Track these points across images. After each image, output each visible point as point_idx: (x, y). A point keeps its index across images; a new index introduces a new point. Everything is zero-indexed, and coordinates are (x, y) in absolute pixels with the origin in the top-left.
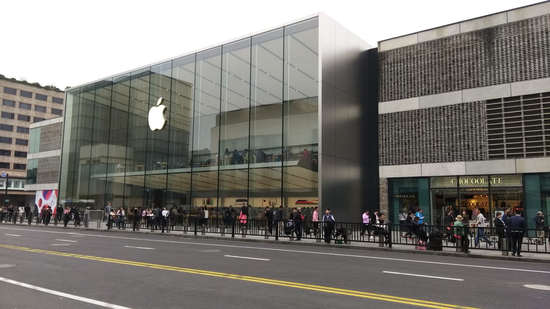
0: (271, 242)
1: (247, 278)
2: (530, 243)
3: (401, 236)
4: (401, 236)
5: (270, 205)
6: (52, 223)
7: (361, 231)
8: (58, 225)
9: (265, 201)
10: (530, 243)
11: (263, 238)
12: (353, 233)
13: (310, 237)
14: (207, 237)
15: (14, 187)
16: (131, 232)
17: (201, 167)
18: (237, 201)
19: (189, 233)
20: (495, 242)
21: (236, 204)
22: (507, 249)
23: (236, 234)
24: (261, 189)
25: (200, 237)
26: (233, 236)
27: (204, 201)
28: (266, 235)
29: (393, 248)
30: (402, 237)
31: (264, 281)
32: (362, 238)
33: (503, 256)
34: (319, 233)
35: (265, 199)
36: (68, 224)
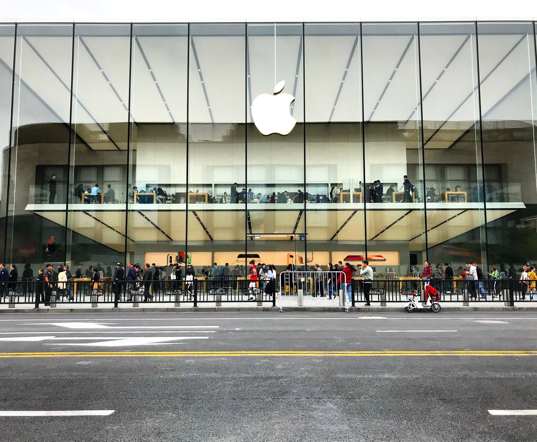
0: (266, 310)
1: (109, 354)
2: (373, 294)
3: (85, 294)
4: (85, 294)
5: (302, 263)
6: (78, 301)
7: (44, 293)
8: (389, 305)
9: (292, 256)
10: (373, 294)
11: (89, 306)
12: (387, 294)
13: (499, 300)
14: (17, 311)
15: (293, 236)
16: (190, 310)
17: (238, 203)
18: (240, 256)
19: (265, 305)
20: (379, 295)
21: (238, 261)
22: (365, 300)
23: (516, 301)
24: (327, 240)
25: (43, 310)
26: (195, 305)
27: (171, 257)
28: (466, 301)
29: (40, 308)
30: (165, 294)
31: (48, 354)
32: (398, 297)
33: (382, 307)
34: (182, 295)
35: (293, 254)
36: (121, 302)
